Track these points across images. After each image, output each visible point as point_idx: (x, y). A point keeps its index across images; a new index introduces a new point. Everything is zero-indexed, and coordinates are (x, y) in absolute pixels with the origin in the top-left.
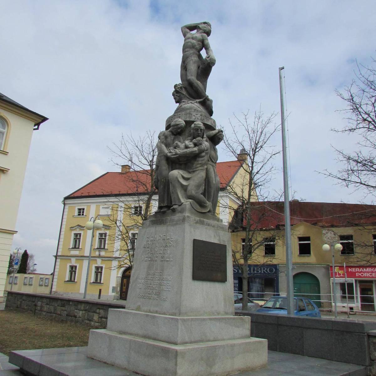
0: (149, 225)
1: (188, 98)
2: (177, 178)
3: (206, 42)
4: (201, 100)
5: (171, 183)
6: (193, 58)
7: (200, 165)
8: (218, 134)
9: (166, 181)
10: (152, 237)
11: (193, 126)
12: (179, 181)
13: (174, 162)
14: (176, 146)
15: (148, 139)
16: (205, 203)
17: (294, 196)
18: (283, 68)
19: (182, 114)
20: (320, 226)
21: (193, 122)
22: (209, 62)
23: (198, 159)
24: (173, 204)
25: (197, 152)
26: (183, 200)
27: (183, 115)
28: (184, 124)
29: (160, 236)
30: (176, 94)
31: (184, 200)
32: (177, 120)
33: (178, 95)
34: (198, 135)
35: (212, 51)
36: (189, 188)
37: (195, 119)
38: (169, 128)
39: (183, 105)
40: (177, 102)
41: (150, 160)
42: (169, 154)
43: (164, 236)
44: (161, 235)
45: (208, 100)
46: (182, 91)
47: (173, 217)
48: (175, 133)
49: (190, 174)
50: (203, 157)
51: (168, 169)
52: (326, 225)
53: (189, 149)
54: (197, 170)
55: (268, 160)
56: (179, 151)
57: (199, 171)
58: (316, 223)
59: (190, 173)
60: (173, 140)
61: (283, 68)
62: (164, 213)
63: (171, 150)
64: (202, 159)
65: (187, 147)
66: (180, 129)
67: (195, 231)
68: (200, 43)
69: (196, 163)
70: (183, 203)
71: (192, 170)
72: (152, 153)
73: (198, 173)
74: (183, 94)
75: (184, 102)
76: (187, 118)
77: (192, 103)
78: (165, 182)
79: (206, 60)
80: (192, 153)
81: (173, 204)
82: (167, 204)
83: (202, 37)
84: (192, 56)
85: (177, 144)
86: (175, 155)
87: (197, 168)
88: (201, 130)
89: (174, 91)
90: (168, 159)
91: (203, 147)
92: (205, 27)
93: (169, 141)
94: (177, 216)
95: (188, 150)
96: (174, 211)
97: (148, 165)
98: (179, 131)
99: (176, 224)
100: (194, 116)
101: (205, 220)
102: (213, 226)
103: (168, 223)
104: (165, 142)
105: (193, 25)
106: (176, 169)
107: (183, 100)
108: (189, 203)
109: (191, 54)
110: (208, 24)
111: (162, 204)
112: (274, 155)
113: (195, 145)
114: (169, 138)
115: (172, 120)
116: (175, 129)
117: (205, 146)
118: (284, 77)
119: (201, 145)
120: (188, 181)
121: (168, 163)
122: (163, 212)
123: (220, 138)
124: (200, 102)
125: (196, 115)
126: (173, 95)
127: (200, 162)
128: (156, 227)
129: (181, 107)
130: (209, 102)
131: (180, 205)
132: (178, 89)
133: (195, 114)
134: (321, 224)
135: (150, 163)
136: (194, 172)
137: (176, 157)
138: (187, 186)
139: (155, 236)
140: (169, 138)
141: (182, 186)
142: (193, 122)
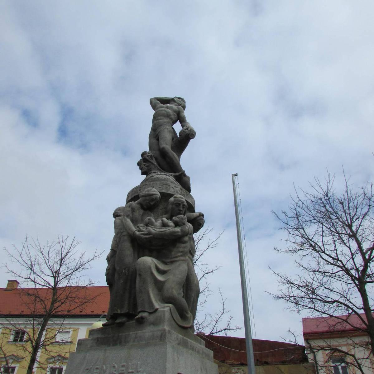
0: (91, 347)
1: (160, 170)
2: (150, 268)
3: (182, 114)
4: (177, 174)
5: (140, 275)
6: (167, 127)
7: (181, 254)
8: (198, 219)
9: (128, 273)
10: (97, 369)
11: (172, 199)
12: (152, 273)
13: (143, 245)
14: (149, 224)
15: (58, 245)
17: (230, 323)
18: (236, 175)
19: (157, 184)
20: (230, 364)
21: (171, 195)
22: (189, 133)
23: (178, 245)
24: (139, 310)
25: (180, 234)
26: (157, 305)
27: (158, 185)
29: (114, 367)
30: (144, 163)
31: (159, 305)
32: (151, 190)
33: (145, 165)
34: (178, 212)
35: (189, 123)
36: (167, 286)
37: (174, 192)
39: (155, 175)
40: (142, 174)
41: (55, 270)
42: (137, 233)
43: (123, 366)
44: (116, 365)
45: (185, 175)
46: (152, 160)
47: (140, 333)
48: (145, 207)
49: (167, 266)
50: (185, 242)
51: (133, 255)
52: (236, 363)
53: (168, 228)
54: (176, 261)
55: (201, 279)
56: (154, 230)
57: (180, 262)
58: (224, 360)
59: (165, 263)
60: (143, 215)
61: (236, 175)
62: (121, 325)
63: (141, 228)
64: (183, 245)
65: (164, 225)
66: (154, 202)
67: (178, 358)
68: (175, 114)
71: (168, 260)
72: (59, 262)
73: (179, 265)
74: (154, 164)
75: (155, 173)
77: (166, 175)
78: (127, 274)
79: (184, 131)
80: (173, 233)
81: (139, 310)
82: (127, 311)
83: (178, 109)
84: (167, 125)
85: (149, 219)
87: (176, 257)
88: (184, 205)
89: (141, 159)
90: (134, 240)
91: (187, 228)
92: (181, 102)
94: (147, 332)
95: (167, 230)
96: (141, 322)
97: (52, 276)
98: (152, 203)
99: (147, 345)
100: (173, 188)
101: (189, 340)
102: (198, 352)
103: (131, 344)
104: (131, 215)
106: (150, 256)
108: (168, 308)
111: (119, 311)
112: (207, 273)
113: (177, 224)
114: (137, 212)
115: (140, 190)
116: (148, 201)
117: (190, 228)
118: (238, 183)
119: (184, 226)
120: (163, 276)
121: (133, 246)
122: (119, 323)
124: (175, 176)
125: (174, 188)
126: (139, 164)
127: (181, 250)
128: (105, 350)
129: (152, 177)
130: (185, 178)
131: (150, 313)
132: (147, 158)
133: (173, 187)
134: (230, 361)
135: (54, 274)
136: (172, 262)
138: (163, 283)
139: (102, 367)
140: (137, 212)
141: (156, 281)
142: (171, 195)
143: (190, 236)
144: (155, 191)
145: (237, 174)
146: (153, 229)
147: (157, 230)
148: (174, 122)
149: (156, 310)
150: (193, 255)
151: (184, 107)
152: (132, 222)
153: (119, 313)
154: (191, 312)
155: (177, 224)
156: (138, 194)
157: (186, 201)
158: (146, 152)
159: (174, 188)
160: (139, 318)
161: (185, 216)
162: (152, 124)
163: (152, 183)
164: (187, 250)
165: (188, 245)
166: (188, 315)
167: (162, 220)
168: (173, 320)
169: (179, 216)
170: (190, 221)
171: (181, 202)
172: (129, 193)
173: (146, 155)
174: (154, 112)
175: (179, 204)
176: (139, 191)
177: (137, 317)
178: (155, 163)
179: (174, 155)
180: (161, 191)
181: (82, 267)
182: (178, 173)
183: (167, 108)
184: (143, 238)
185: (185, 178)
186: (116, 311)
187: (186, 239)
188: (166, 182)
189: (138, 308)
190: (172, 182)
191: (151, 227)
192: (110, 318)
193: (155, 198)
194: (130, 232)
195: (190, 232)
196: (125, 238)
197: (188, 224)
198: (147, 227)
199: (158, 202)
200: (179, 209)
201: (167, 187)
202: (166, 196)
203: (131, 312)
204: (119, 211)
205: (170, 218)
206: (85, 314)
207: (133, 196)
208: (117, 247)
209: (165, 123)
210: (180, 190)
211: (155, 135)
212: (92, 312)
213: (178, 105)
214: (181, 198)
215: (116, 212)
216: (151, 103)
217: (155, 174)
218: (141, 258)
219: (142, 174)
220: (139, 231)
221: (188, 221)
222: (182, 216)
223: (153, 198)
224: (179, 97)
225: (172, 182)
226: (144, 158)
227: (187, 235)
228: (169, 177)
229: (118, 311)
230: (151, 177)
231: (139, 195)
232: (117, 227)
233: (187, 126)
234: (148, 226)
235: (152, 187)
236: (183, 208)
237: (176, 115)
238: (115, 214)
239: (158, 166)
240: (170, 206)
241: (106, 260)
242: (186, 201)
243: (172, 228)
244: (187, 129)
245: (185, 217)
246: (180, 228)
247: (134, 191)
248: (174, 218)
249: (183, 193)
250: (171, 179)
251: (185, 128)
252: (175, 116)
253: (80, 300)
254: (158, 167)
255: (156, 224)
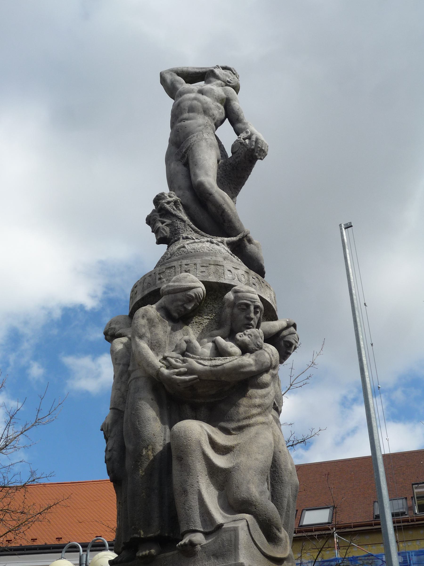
1: (196, 232)
7: (259, 410)
8: (285, 333)
11: (230, 295)
13: (183, 398)
16: (279, 531)
19: (195, 264)
21: (228, 287)
24: (184, 528)
25: (254, 368)
27: (198, 266)
28: (116, 332)
34: (246, 322)
38: (159, 300)
39: (188, 244)
40: (160, 241)
42: (165, 371)
48: (175, 315)
50: (264, 386)
53: (229, 359)
54: (249, 426)
59: (227, 431)
63: (173, 361)
65: (219, 352)
68: (219, 105)
69: (244, 401)
70: (222, 525)
71: (231, 425)
74: (184, 221)
75: (187, 238)
76: (210, 275)
77: (212, 242)
79: (241, 143)
80: (237, 370)
86: (184, 374)
87: (249, 418)
88: (256, 307)
89: (154, 211)
91: (267, 355)
93: (161, 336)
105: (198, 71)
106: (196, 418)
107: (184, 235)
109: (200, 126)
110: (232, 71)
111: (142, 533)
113: (245, 349)
115: (160, 279)
116: (180, 303)
119: (260, 351)
123: (291, 344)
124: (229, 244)
125: (233, 270)
126: (150, 221)
127: (257, 401)
132: (167, 206)
136: (240, 429)
137: (191, 380)
141: (213, 471)
143: (274, 372)
144: (193, 281)
145: (350, 223)
146: (196, 361)
147: (206, 363)
148: (218, 124)
149: (220, 526)
150: (279, 410)
151: (236, 88)
152: (152, 349)
153: (142, 536)
154: (285, 529)
155: (245, 349)
156: (156, 288)
157: (261, 297)
158: (163, 194)
159: (233, 270)
160: (185, 544)
161: (260, 329)
162: (169, 130)
163: (184, 262)
164: (268, 401)
165: (270, 390)
166: (281, 533)
167: (214, 342)
168: (255, 547)
169: (249, 331)
170: (272, 338)
171: (251, 301)
172: (135, 286)
173: (164, 201)
174: (170, 102)
175: (248, 306)
176: (158, 282)
177: (182, 542)
178: (186, 218)
179: (224, 198)
180: (206, 280)
181: (12, 444)
182: (235, 236)
183: (201, 92)
184: (178, 382)
185: (249, 247)
186: (137, 533)
187: (266, 378)
188: (214, 258)
189: (181, 525)
190: (225, 258)
191: (193, 358)
192: (123, 549)
193: (195, 294)
194: (151, 371)
195: (274, 363)
196: (141, 383)
197: (268, 347)
198: (185, 358)
199: (200, 303)
200: (248, 316)
201: (217, 271)
202: (216, 290)
203: (166, 535)
204: (117, 326)
205: (231, 336)
206: (44, 543)
207: (146, 292)
208: (124, 402)
209: (200, 128)
210: (246, 275)
211: (181, 153)
212: (59, 539)
213: (223, 83)
214: (249, 292)
215: (112, 328)
216: (163, 81)
217: (188, 242)
218: (175, 425)
219: (160, 241)
220: (167, 368)
221: (266, 341)
222: (254, 330)
223: (191, 296)
224: (224, 65)
225: (225, 258)
226: (161, 207)
227: (266, 371)
228: (218, 248)
229: (140, 534)
230: (179, 248)
231: (159, 289)
232: (118, 362)
233: (247, 132)
234: (186, 356)
235: (186, 271)
236: (256, 313)
237: (222, 107)
238: (109, 333)
239: (191, 223)
240: (228, 310)
241: (102, 430)
242: (261, 297)
243: (236, 359)
244: (249, 138)
245: (260, 330)
246: (253, 356)
247: (147, 281)
248: (239, 336)
249: (252, 281)
250: (223, 250)
251: (243, 135)
252: (221, 111)
253: (15, 516)
254: (193, 226)
255: (200, 349)
